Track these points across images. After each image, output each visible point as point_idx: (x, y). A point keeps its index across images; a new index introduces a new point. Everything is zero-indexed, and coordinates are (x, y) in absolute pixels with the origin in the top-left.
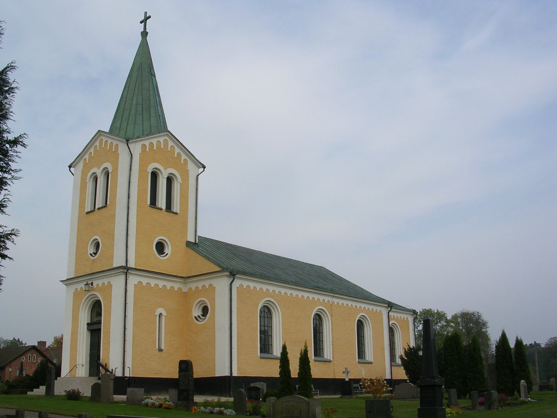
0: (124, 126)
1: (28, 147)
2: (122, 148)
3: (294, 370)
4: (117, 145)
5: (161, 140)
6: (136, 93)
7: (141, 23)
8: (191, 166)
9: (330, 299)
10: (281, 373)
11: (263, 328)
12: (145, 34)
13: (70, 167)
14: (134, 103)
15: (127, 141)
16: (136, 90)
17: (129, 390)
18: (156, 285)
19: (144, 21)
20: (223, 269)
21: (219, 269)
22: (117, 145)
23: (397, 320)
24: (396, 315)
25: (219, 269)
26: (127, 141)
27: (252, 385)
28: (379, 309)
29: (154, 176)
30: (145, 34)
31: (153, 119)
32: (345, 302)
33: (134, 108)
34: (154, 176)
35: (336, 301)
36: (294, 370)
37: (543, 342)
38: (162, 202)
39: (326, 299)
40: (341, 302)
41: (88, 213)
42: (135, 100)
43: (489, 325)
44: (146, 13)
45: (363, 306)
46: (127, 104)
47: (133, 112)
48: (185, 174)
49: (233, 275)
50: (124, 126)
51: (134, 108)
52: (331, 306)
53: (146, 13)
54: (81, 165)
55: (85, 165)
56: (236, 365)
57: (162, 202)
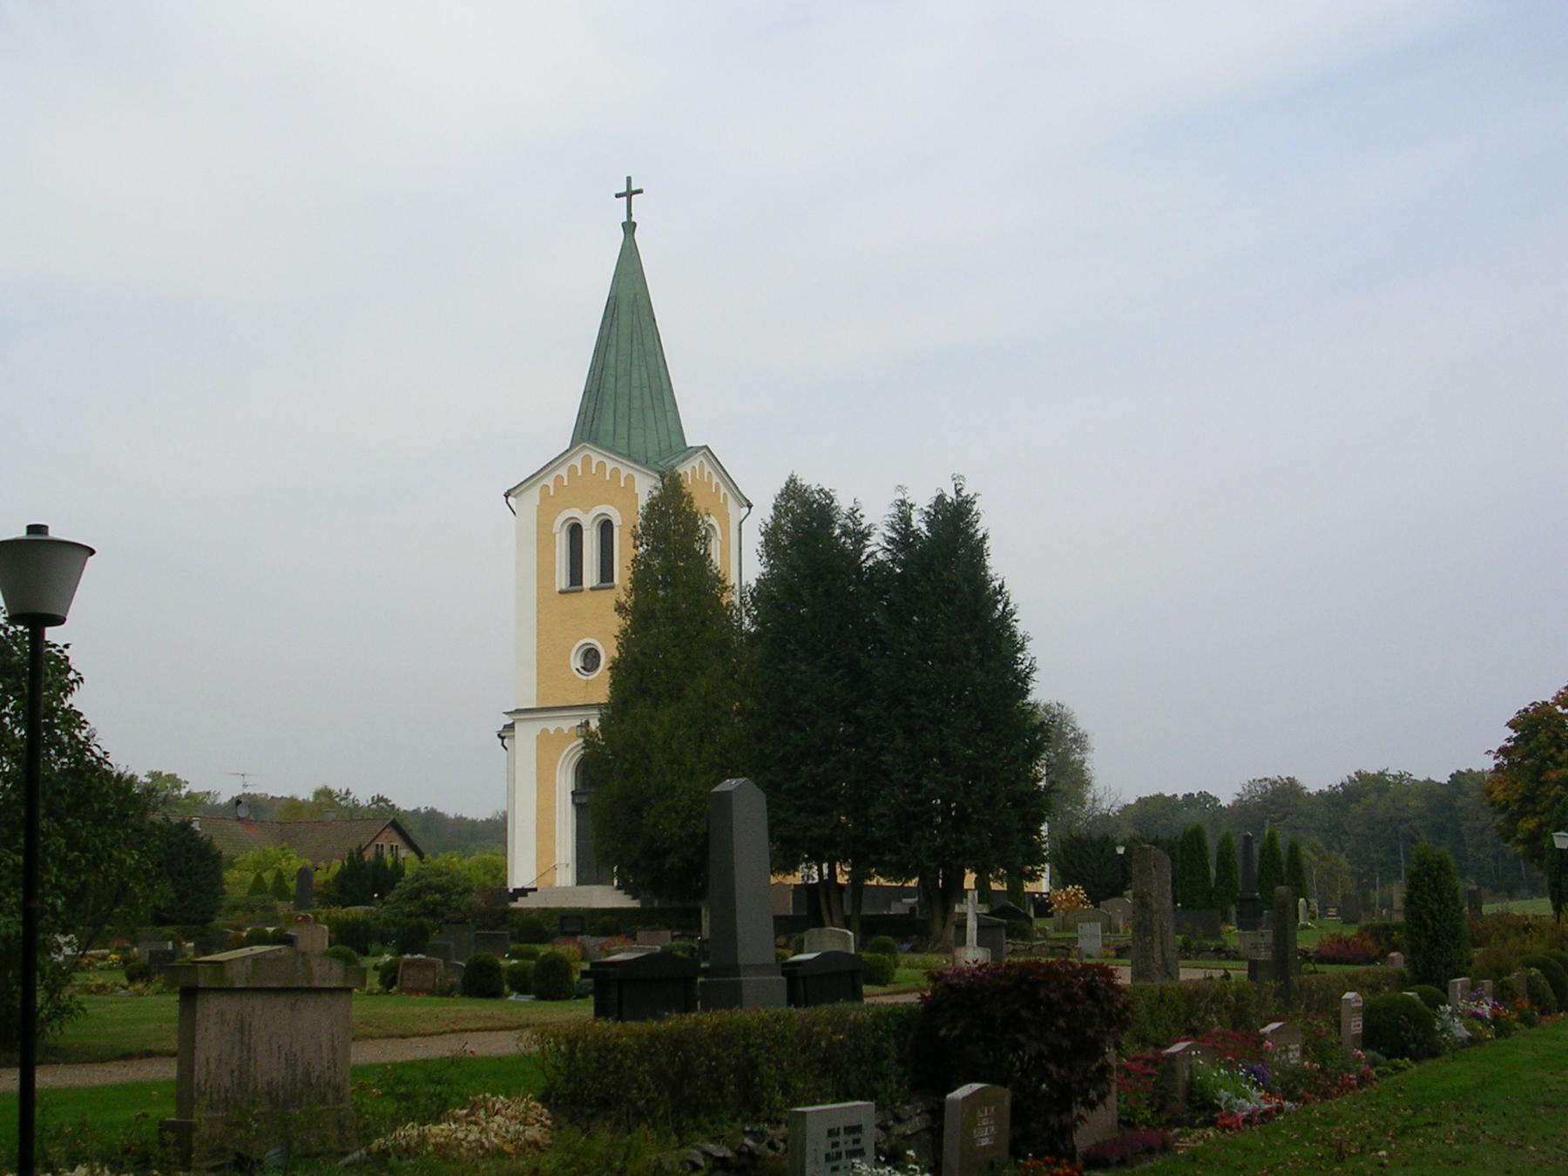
0: (622, 430)
1: (958, 471)
6: (635, 362)
7: (640, 192)
8: (732, 505)
11: (1113, 953)
12: (629, 227)
13: (507, 496)
18: (559, 730)
19: (629, 194)
22: (630, 478)
29: (575, 531)
30: (629, 227)
33: (636, 392)
34: (575, 531)
37: (451, 815)
38: (590, 575)
41: (561, 592)
42: (635, 376)
44: (629, 179)
46: (620, 384)
47: (636, 404)
50: (622, 430)
53: (629, 179)
54: (533, 496)
56: (532, 856)
57: (590, 575)
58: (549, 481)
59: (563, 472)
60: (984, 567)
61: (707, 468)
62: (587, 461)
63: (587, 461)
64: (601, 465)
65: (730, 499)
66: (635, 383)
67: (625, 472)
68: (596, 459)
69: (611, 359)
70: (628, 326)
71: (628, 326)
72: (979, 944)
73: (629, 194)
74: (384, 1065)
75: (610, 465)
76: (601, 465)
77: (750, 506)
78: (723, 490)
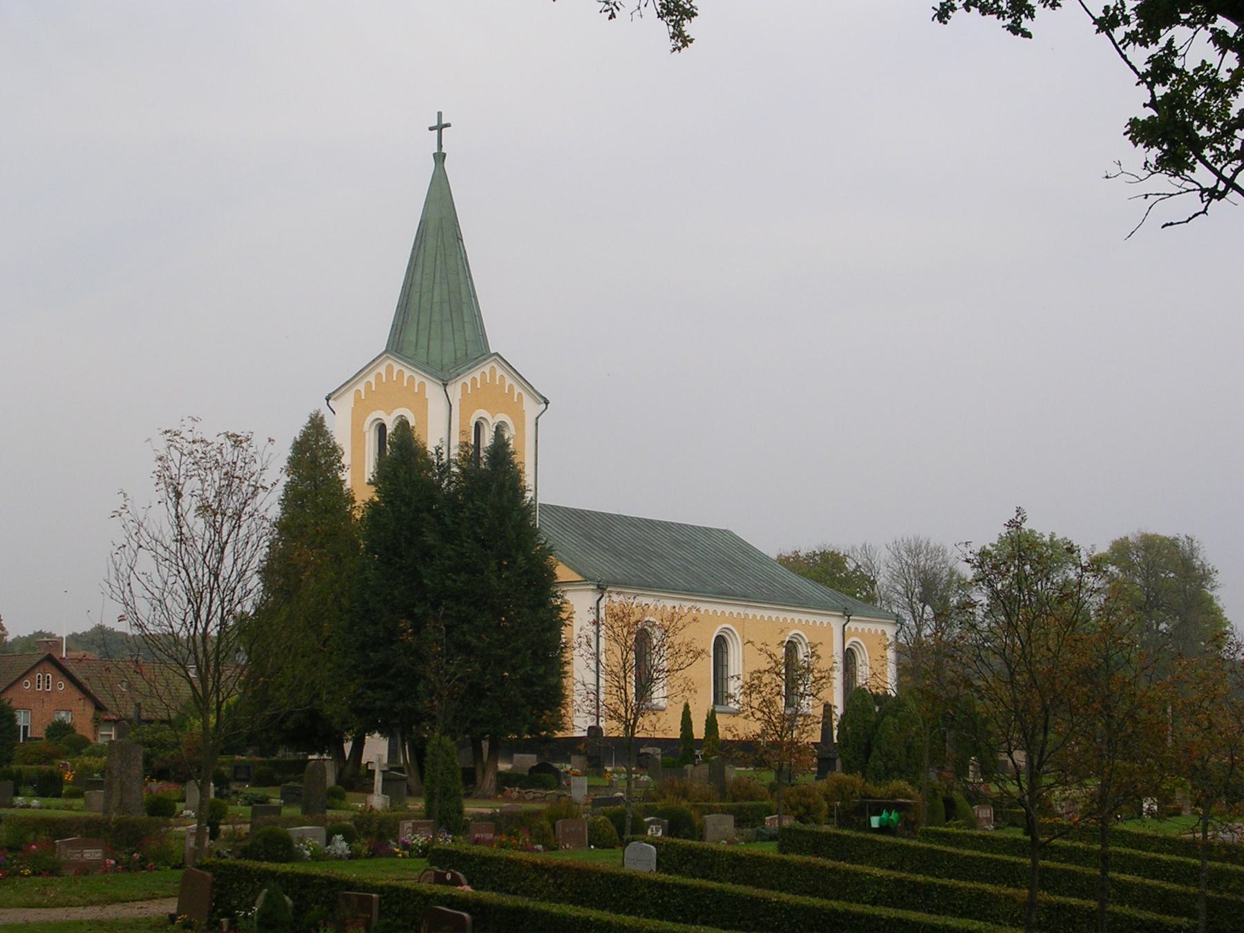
0: (423, 341)
2: (433, 391)
3: (699, 731)
4: (422, 384)
5: (487, 369)
6: (437, 280)
7: (431, 129)
9: (742, 610)
10: (18, 640)
12: (440, 157)
14: (437, 299)
15: (445, 385)
16: (437, 275)
17: (517, 756)
19: (440, 127)
20: (587, 579)
21: (580, 578)
22: (422, 384)
23: (862, 635)
24: (860, 626)
25: (580, 578)
26: (445, 385)
27: (642, 751)
28: (825, 620)
30: (440, 157)
31: (468, 327)
32: (766, 614)
33: (436, 308)
35: (751, 612)
36: (699, 731)
39: (735, 610)
40: (759, 613)
42: (437, 292)
43: (1218, 579)
44: (440, 114)
45: (797, 617)
46: (423, 300)
47: (436, 317)
48: (519, 418)
49: (601, 589)
50: (423, 341)
51: (436, 308)
52: (742, 622)
53: (440, 114)
55: (358, 400)
58: (361, 387)
59: (371, 378)
60: (520, 480)
61: (499, 372)
62: (390, 370)
63: (390, 370)
64: (401, 373)
65: (526, 397)
66: (437, 299)
67: (418, 379)
68: (397, 367)
69: (418, 276)
70: (439, 244)
71: (439, 244)
72: (383, 792)
73: (440, 127)
74: (705, 923)
75: (407, 373)
76: (401, 373)
77: (547, 403)
78: (517, 390)
